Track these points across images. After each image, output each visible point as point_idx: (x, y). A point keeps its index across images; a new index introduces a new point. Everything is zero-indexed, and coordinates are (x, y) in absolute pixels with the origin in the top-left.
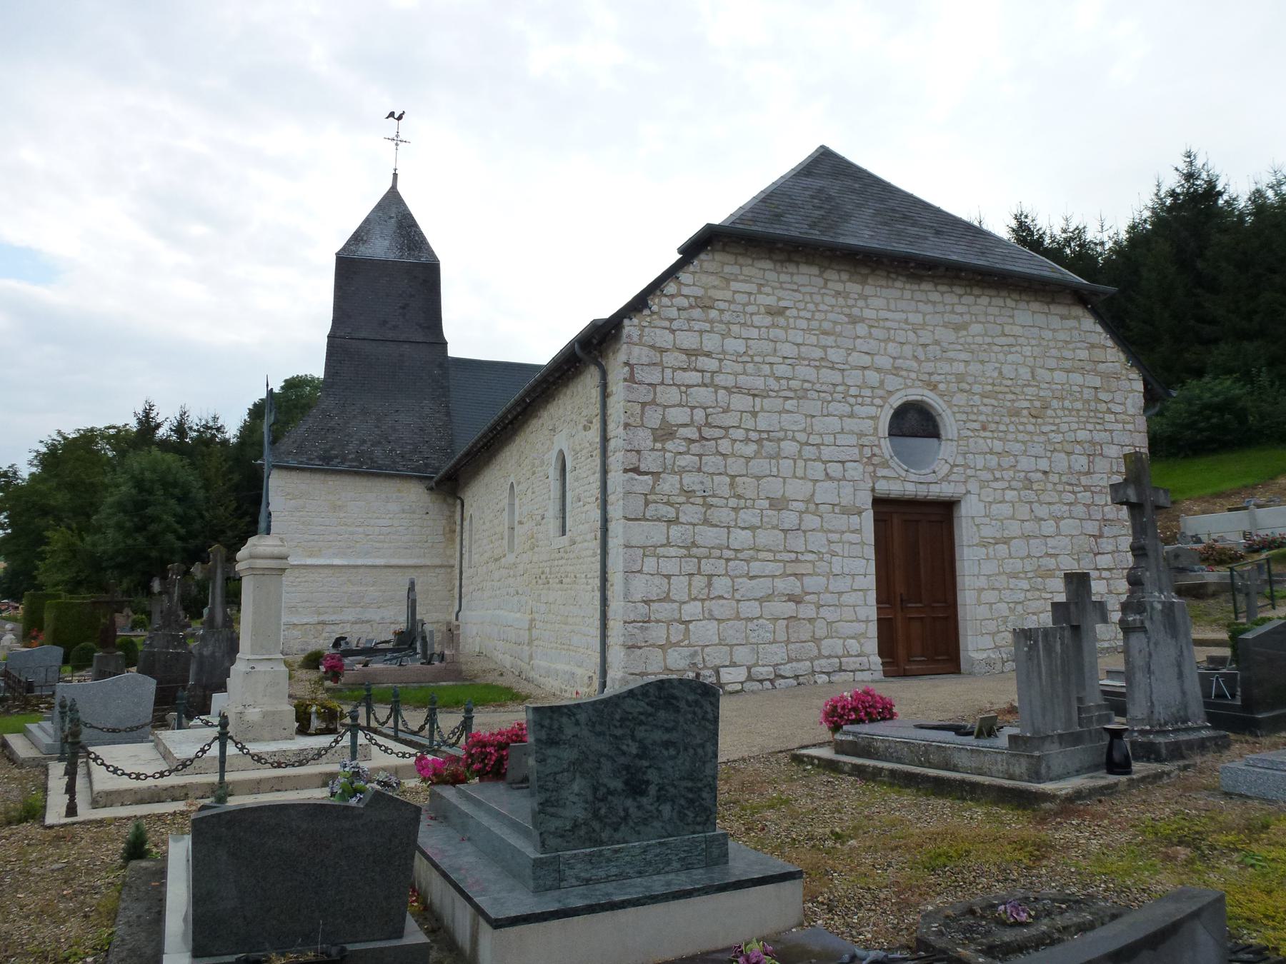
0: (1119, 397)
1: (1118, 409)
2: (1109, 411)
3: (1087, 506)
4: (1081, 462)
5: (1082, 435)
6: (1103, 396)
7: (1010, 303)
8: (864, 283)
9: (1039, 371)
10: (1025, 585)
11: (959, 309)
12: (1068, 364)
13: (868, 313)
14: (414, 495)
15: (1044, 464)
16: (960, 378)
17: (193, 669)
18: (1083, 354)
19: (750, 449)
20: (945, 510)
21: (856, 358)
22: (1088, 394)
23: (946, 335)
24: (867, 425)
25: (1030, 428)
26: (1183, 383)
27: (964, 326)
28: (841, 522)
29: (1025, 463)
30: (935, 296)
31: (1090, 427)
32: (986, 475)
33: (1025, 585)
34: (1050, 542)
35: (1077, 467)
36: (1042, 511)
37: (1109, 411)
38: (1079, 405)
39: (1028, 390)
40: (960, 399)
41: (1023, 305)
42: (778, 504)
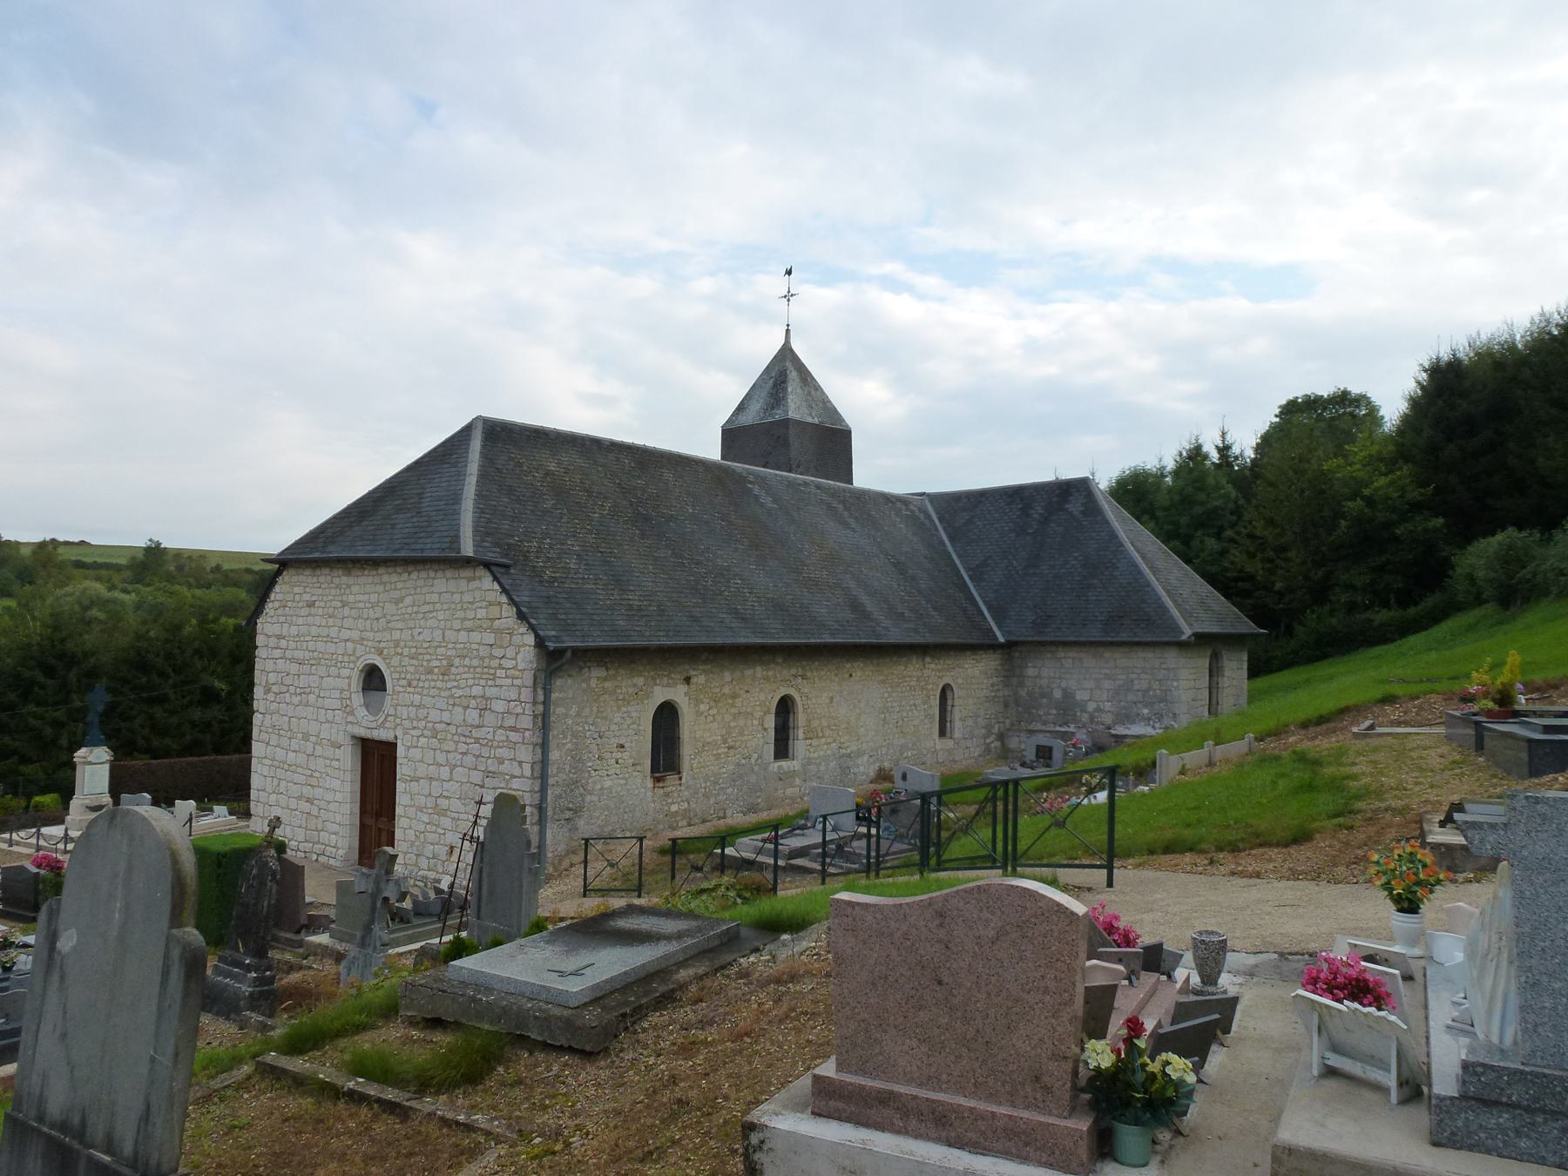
0: (510, 652)
1: (509, 664)
2: (500, 667)
3: (477, 757)
4: (473, 716)
5: (476, 691)
6: (498, 652)
7: (432, 574)
8: (349, 575)
9: (448, 633)
10: (425, 818)
11: (400, 585)
12: (468, 624)
13: (351, 598)
14: (522, 651)
15: (446, 717)
16: (397, 644)
17: (236, 757)
18: (481, 613)
19: (296, 700)
20: (392, 746)
21: (345, 634)
22: (484, 651)
23: (390, 608)
24: (344, 683)
25: (439, 684)
26: (211, 810)
27: (401, 600)
28: (330, 752)
29: (434, 715)
30: (386, 578)
31: (483, 682)
32: (407, 724)
33: (425, 818)
34: (446, 785)
35: (470, 721)
36: (441, 758)
37: (500, 667)
38: (475, 662)
39: (441, 651)
40: (395, 661)
41: (440, 574)
42: (306, 737)
